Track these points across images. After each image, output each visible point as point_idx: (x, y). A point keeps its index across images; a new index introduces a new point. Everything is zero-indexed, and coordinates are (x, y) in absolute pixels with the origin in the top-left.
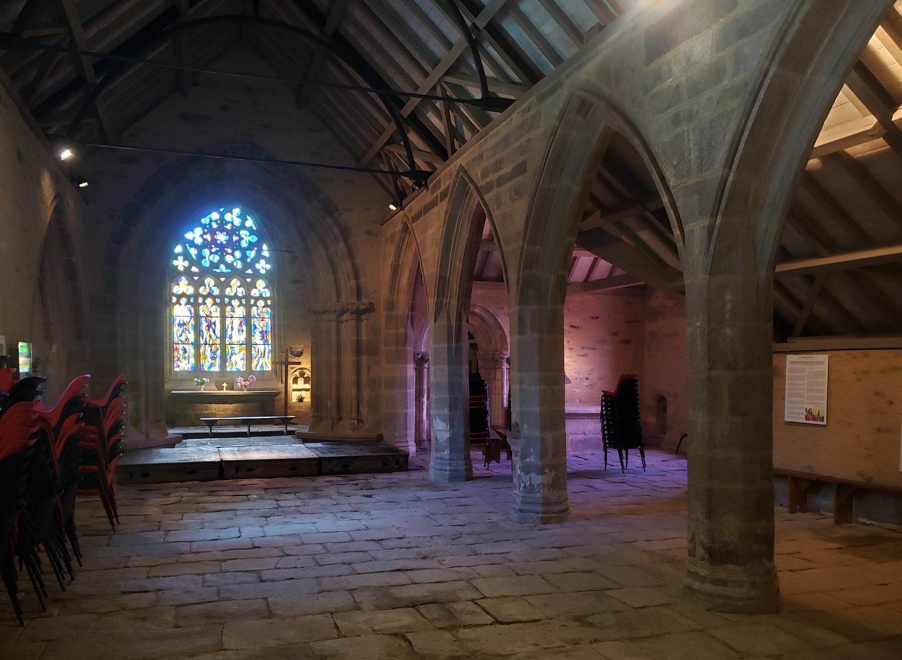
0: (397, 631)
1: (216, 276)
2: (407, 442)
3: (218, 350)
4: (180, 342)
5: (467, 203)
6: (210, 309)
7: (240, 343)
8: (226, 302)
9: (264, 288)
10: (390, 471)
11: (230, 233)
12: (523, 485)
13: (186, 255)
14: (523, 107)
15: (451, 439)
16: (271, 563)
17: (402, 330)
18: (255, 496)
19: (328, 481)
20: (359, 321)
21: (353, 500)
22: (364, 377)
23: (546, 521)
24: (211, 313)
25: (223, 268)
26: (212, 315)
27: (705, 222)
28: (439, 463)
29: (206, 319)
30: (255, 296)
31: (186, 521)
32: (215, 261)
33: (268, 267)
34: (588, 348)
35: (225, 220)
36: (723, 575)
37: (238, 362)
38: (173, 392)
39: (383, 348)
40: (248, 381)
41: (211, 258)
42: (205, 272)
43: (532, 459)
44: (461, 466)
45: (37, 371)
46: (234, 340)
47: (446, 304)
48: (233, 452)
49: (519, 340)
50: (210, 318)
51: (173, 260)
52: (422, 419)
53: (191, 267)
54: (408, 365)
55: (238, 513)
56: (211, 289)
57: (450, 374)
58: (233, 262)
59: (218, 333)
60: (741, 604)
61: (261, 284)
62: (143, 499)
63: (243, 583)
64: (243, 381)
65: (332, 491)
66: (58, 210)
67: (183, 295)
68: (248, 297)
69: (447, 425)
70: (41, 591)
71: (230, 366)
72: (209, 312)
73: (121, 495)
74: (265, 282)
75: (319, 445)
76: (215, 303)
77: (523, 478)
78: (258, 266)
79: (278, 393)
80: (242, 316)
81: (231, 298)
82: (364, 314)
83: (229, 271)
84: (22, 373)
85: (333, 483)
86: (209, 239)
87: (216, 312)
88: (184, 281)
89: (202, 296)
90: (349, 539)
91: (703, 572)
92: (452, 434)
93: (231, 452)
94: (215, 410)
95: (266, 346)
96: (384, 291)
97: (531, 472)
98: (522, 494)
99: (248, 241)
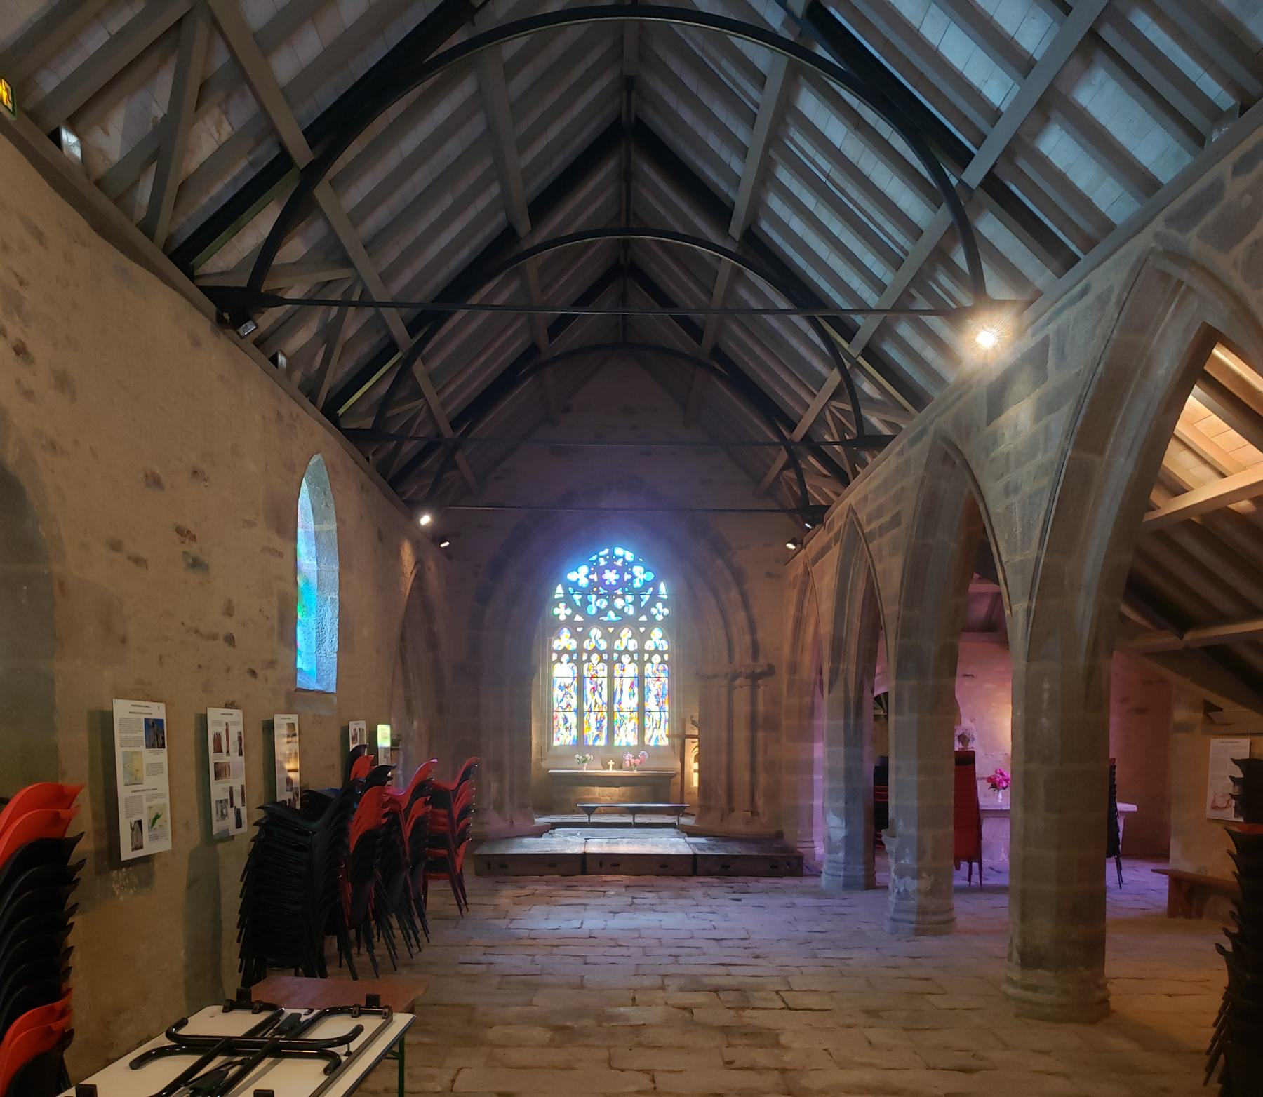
0: (687, 1006)
1: (604, 626)
2: (813, 842)
4: (560, 709)
7: (631, 710)
8: (615, 659)
9: (661, 639)
10: (780, 876)
11: (621, 571)
12: (896, 891)
13: (568, 600)
15: (848, 840)
16: (601, 950)
17: (807, 699)
18: (612, 893)
19: (700, 882)
20: (754, 687)
21: (718, 901)
23: (920, 932)
24: (597, 672)
25: (611, 616)
26: (598, 675)
27: (1024, 604)
29: (591, 679)
31: (532, 912)
32: (603, 607)
33: (666, 611)
37: (626, 736)
38: (550, 771)
40: (639, 758)
41: (598, 603)
42: (590, 621)
44: (859, 870)
45: (398, 749)
46: (624, 706)
47: (843, 670)
48: (601, 844)
50: (595, 679)
51: (554, 608)
55: (588, 907)
56: (597, 642)
58: (624, 607)
59: (605, 698)
61: (657, 633)
63: (568, 964)
64: (633, 758)
65: (699, 893)
66: (419, 577)
67: (565, 650)
68: (641, 651)
69: (842, 820)
70: (394, 957)
73: (470, 882)
74: (663, 632)
75: (702, 840)
76: (601, 660)
78: (654, 611)
79: (673, 776)
81: (621, 653)
82: (760, 679)
83: (620, 618)
84: (381, 748)
85: (704, 884)
86: (596, 580)
87: (602, 670)
88: (566, 633)
89: (586, 651)
90: (689, 936)
91: (1016, 977)
93: (598, 844)
96: (787, 648)
99: (642, 581)
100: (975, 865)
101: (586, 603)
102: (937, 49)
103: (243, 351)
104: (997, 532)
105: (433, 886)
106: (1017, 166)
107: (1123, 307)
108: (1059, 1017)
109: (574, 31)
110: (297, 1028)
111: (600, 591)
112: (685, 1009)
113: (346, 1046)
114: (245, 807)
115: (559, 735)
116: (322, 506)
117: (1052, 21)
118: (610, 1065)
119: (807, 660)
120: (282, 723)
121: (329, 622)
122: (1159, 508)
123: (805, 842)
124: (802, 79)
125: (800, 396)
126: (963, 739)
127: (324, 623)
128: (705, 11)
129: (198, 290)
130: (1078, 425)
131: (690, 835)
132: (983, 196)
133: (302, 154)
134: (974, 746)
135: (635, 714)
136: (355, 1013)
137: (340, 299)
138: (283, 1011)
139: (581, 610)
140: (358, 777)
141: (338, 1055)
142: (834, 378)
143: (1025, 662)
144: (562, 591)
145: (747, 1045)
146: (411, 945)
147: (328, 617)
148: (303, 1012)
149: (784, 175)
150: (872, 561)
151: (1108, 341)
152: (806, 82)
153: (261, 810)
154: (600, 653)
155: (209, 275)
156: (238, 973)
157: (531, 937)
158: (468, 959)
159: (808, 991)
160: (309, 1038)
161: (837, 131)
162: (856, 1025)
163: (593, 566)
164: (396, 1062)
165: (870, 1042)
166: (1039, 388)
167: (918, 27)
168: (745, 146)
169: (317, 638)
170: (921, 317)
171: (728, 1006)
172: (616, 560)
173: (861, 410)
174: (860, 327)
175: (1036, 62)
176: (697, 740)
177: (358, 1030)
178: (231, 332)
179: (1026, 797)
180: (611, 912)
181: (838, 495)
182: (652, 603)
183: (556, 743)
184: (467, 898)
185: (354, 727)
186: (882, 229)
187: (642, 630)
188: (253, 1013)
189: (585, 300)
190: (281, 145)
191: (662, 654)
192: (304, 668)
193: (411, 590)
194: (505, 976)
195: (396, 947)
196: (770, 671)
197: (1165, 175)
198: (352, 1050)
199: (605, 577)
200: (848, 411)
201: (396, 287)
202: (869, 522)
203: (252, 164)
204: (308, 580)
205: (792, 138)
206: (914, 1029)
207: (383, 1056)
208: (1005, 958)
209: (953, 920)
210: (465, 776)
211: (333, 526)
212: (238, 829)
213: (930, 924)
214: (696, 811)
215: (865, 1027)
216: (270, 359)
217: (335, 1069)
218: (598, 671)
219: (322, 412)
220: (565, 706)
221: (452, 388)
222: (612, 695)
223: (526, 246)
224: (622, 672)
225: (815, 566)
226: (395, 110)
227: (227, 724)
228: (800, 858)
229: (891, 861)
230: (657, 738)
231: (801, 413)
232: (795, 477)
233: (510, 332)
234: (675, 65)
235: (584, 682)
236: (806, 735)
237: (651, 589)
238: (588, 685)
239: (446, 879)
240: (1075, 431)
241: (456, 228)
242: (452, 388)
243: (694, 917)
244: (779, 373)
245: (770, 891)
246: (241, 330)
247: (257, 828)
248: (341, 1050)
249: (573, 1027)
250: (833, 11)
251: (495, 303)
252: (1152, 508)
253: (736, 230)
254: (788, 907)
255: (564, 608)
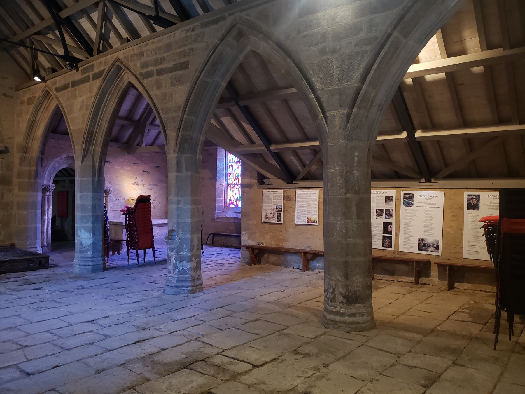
2: (37, 248)
5: (117, 83)
14: (188, 27)
15: (93, 244)
28: (83, 261)
34: (153, 185)
36: (354, 311)
39: (16, 180)
47: (91, 150)
52: (44, 231)
57: (93, 199)
60: (364, 325)
77: (177, 265)
92: (94, 240)
97: (184, 261)
213: (196, 286)
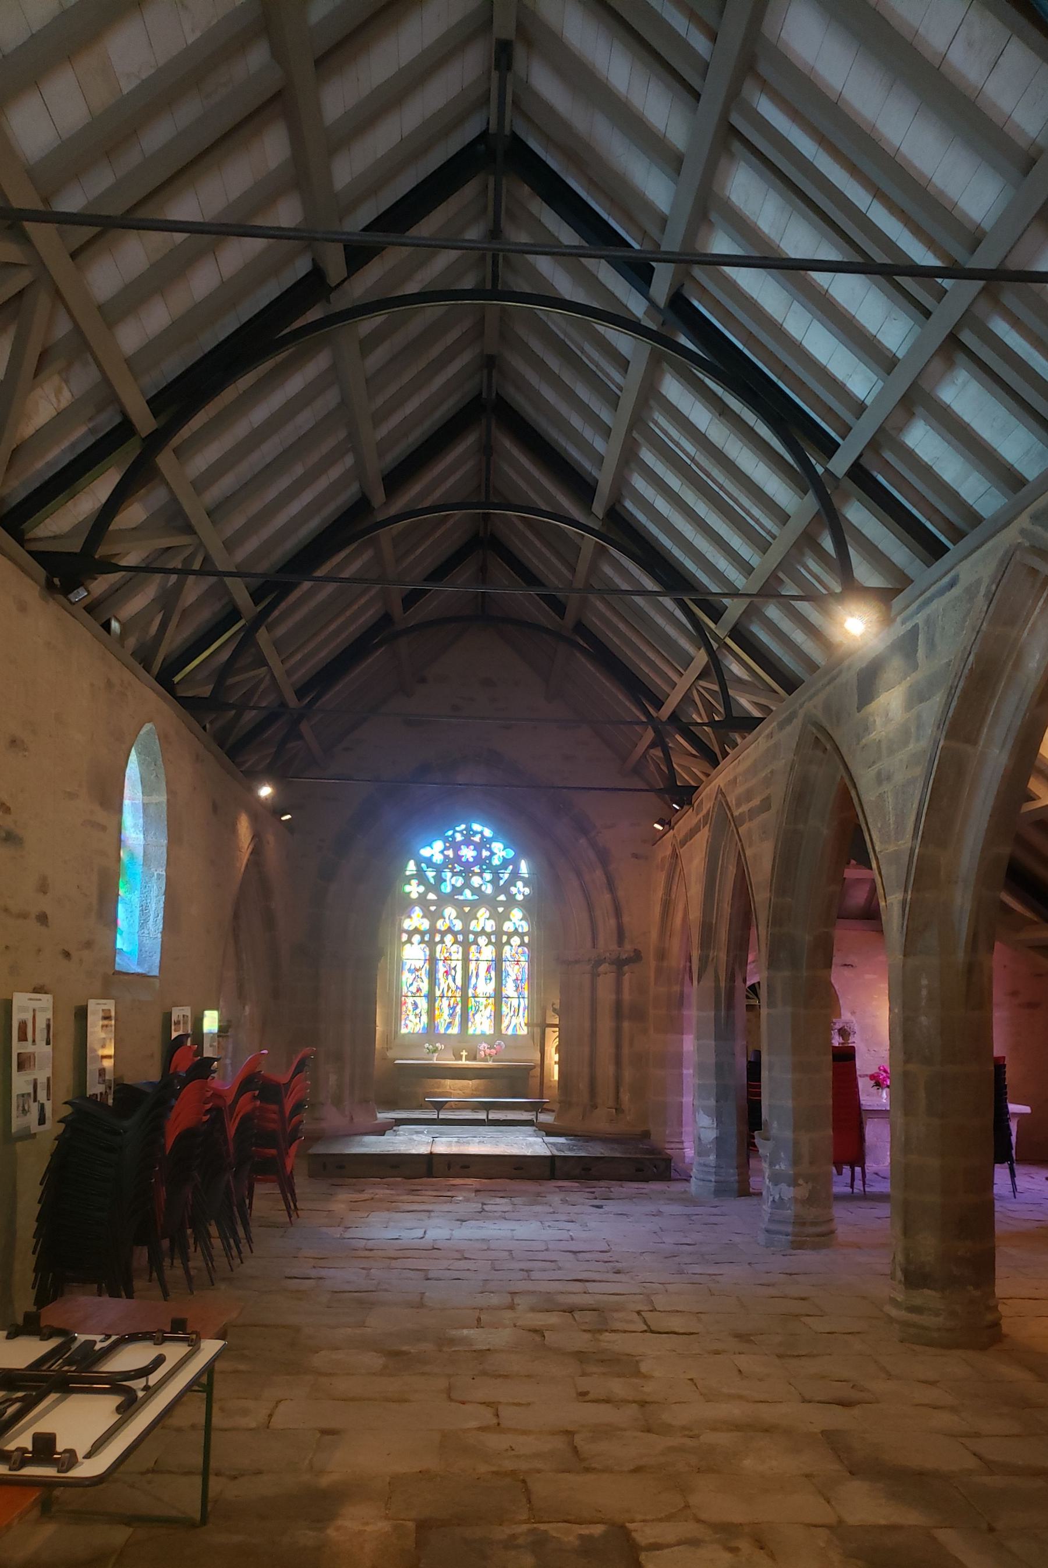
0: (537, 1328)
1: (459, 905)
2: (682, 1142)
3: (457, 1004)
4: (409, 994)
6: (450, 949)
7: (488, 995)
9: (521, 920)
10: (646, 1180)
11: (478, 847)
12: (771, 1199)
13: (420, 876)
16: (445, 1264)
17: (676, 988)
18: (460, 1198)
21: (576, 1209)
22: (626, 1050)
24: (450, 954)
25: (468, 894)
30: (509, 931)
32: (459, 885)
33: (527, 891)
35: (472, 830)
36: (918, 1301)
37: (482, 1024)
38: (396, 1062)
40: (495, 1048)
41: (453, 881)
43: (782, 1167)
44: (732, 1175)
46: (480, 991)
47: (713, 959)
48: (450, 1144)
49: (768, 1014)
50: (449, 962)
53: (428, 894)
54: (684, 1036)
55: (432, 1214)
56: (451, 922)
61: (517, 914)
62: (331, 1195)
65: (556, 1199)
66: (257, 851)
67: (416, 931)
68: (499, 932)
69: (713, 1121)
71: (473, 1028)
72: (448, 954)
73: (302, 1184)
75: (562, 1140)
76: (456, 942)
78: (513, 890)
79: (534, 1067)
80: (490, 959)
81: (477, 934)
82: (627, 965)
83: (476, 897)
85: (563, 1189)
86: (451, 856)
87: (457, 952)
88: (417, 912)
89: (439, 932)
90: (544, 1248)
91: (900, 1298)
94: (450, 1087)
95: (521, 1000)
96: (654, 934)
98: (770, 1210)
100: (858, 1169)
101: (439, 880)
102: (801, 343)
103: (73, 616)
104: (870, 820)
105: (260, 1189)
106: (883, 457)
107: (992, 600)
108: (947, 1342)
109: (433, 311)
110: (91, 1356)
111: (455, 868)
112: (535, 1331)
113: (145, 1379)
114: (51, 1101)
115: (408, 1022)
116: (152, 777)
117: (913, 323)
118: (449, 1397)
119: (675, 946)
120: (96, 1008)
121: (154, 901)
122: (1040, 798)
123: (672, 1142)
124: (665, 365)
125: (666, 674)
126: (844, 1033)
127: (149, 901)
128: (568, 298)
129: (27, 554)
130: (950, 714)
131: (548, 1134)
132: (849, 485)
133: (145, 422)
134: (856, 1041)
135: (492, 1000)
136: (158, 1338)
137: (180, 567)
138: (76, 1338)
139: (435, 888)
140: (178, 1070)
141: (135, 1391)
142: (701, 658)
143: (901, 957)
144: (414, 868)
145: (604, 1374)
146: (232, 1257)
147: (154, 893)
148: (98, 1338)
149: (648, 456)
150: (742, 845)
151: (978, 632)
152: (668, 367)
153: (67, 1105)
154: (455, 934)
155: (40, 539)
156: (31, 1290)
157: (367, 1248)
158: (295, 1272)
159: (672, 1311)
160: (101, 1370)
161: (701, 416)
162: (725, 1351)
163: (449, 842)
164: (205, 1394)
165: (740, 1371)
166: (909, 676)
167: (781, 322)
168: (609, 426)
169: (140, 917)
170: (793, 602)
171: (584, 1328)
172: (474, 835)
173: (729, 690)
174: (727, 607)
175: (899, 360)
176: (557, 1029)
177: (160, 1360)
178: (61, 597)
179: (906, 1101)
180: (458, 1220)
181: (708, 775)
182: (511, 882)
183: (404, 1031)
184: (297, 1204)
185: (177, 1013)
186: (748, 513)
187: (501, 910)
188: (41, 1340)
189: (438, 574)
190: (124, 414)
191: (522, 935)
192: (124, 949)
193: (247, 865)
194: (336, 1292)
195: (215, 1258)
196: (637, 957)
197: (1031, 472)
198: (151, 1383)
199: (461, 853)
200: (715, 691)
201: (241, 554)
202: (739, 805)
203: (92, 431)
204: (132, 854)
205: (657, 421)
206: (790, 1356)
207: (188, 1388)
208: (888, 1275)
209: (832, 1232)
210: (300, 1068)
211: (163, 798)
212: (41, 1126)
214: (556, 1107)
215: (735, 1354)
216: (101, 626)
217: (129, 1407)
218: (452, 953)
219: (156, 679)
220: (415, 991)
221: (298, 656)
222: (466, 977)
223: (380, 517)
224: (478, 955)
225: (683, 849)
226: (245, 382)
227: (34, 1010)
228: (668, 1160)
229: (765, 1166)
230: (515, 1026)
231: (668, 692)
232: (661, 755)
233: (362, 601)
234: (536, 345)
235: (436, 964)
236: (675, 1026)
237: (511, 867)
238: (441, 968)
239: (274, 1182)
240: (947, 723)
241: (307, 497)
242: (298, 656)
243: (549, 1226)
244: (644, 650)
245: (635, 1198)
246: (71, 596)
247: (62, 1126)
248: (138, 1384)
249: (410, 1353)
250: (696, 303)
251: (342, 576)
252: (1031, 798)
253: (599, 508)
254: (653, 1215)
255: (416, 885)
